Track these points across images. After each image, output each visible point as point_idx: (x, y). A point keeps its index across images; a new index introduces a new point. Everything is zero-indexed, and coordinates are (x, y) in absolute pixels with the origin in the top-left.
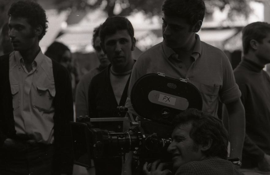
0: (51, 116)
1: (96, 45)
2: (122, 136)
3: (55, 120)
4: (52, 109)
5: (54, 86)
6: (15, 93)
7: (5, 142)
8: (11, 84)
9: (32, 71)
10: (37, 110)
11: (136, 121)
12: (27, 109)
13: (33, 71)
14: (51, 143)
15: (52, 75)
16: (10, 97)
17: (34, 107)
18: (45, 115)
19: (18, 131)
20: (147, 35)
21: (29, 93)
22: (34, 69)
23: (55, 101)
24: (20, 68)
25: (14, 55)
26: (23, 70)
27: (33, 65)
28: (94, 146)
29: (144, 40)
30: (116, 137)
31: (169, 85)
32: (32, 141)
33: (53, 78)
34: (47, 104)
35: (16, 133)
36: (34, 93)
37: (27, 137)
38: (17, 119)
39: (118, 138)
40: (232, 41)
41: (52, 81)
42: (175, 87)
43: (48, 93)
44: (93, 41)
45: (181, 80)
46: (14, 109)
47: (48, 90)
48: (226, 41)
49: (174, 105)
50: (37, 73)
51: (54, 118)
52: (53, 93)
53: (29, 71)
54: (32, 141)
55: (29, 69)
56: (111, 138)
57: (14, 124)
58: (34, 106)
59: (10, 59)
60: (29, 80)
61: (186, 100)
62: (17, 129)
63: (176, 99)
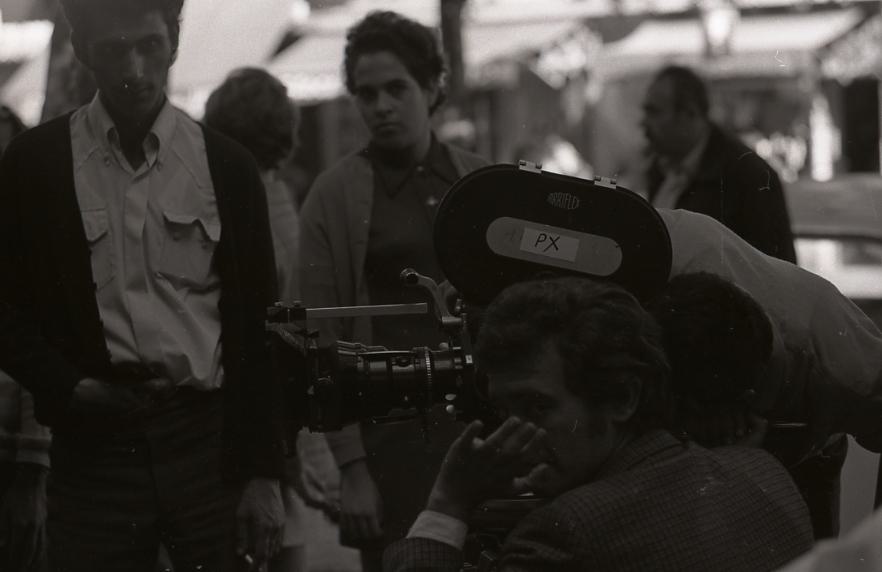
0: (212, 300)
1: (358, 83)
2: (404, 361)
3: (225, 315)
4: (213, 280)
5: (214, 209)
6: (98, 236)
7: (77, 389)
8: (82, 208)
9: (145, 164)
10: (167, 286)
11: (456, 315)
12: (137, 285)
13: (148, 165)
14: (218, 386)
15: (207, 173)
16: (79, 249)
17: (160, 278)
18: (195, 299)
19: (117, 352)
20: (571, 36)
21: (140, 234)
22: (151, 159)
23: (223, 257)
24: (106, 159)
25: (84, 117)
26: (114, 161)
27: (146, 146)
28: (311, 391)
29: (563, 53)
30: (382, 365)
31: (555, 199)
32: (159, 383)
33: (211, 184)
34: (196, 263)
35: (112, 360)
36: (157, 234)
37: (141, 372)
38: (109, 319)
39: (389, 366)
40: (847, 48)
41: (207, 194)
42: (575, 204)
43: (197, 230)
44: (344, 67)
45: (521, 168)
46: (98, 287)
47: (197, 223)
48: (827, 49)
49: (572, 259)
50: (159, 170)
51: (220, 304)
52: (215, 232)
53: (136, 168)
54: (159, 383)
55: (136, 156)
56: (367, 367)
57: (100, 332)
58: (159, 275)
59: (72, 133)
60: (137, 195)
61: (613, 243)
62: (111, 346)
63: (578, 241)
